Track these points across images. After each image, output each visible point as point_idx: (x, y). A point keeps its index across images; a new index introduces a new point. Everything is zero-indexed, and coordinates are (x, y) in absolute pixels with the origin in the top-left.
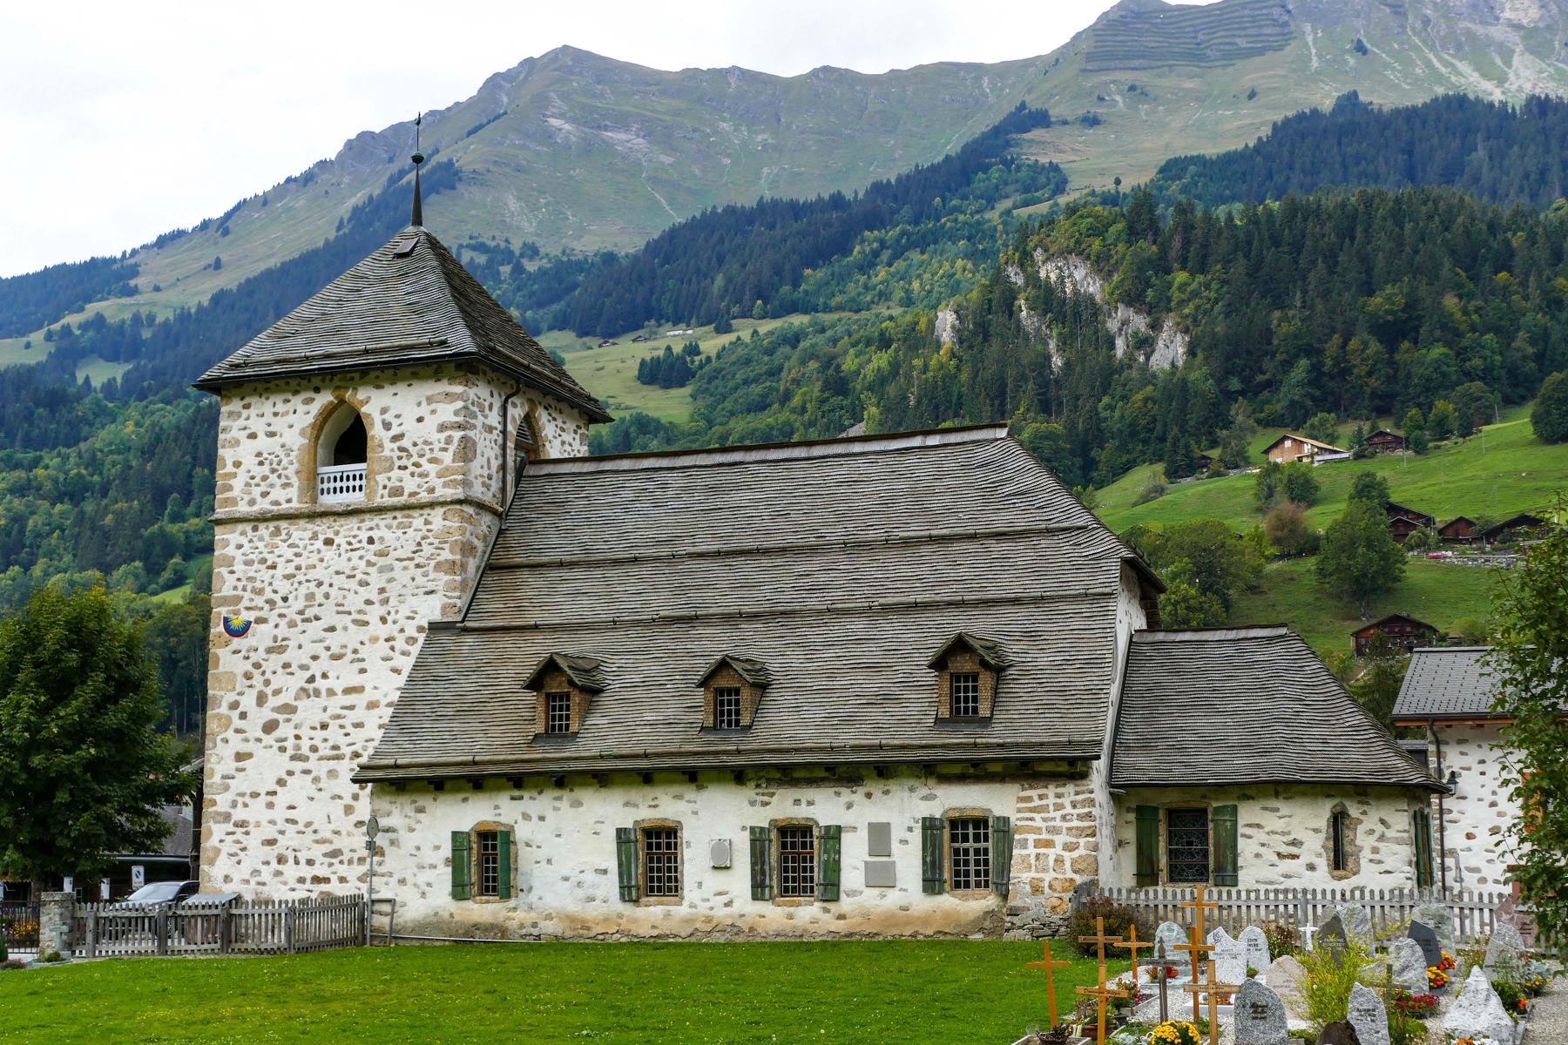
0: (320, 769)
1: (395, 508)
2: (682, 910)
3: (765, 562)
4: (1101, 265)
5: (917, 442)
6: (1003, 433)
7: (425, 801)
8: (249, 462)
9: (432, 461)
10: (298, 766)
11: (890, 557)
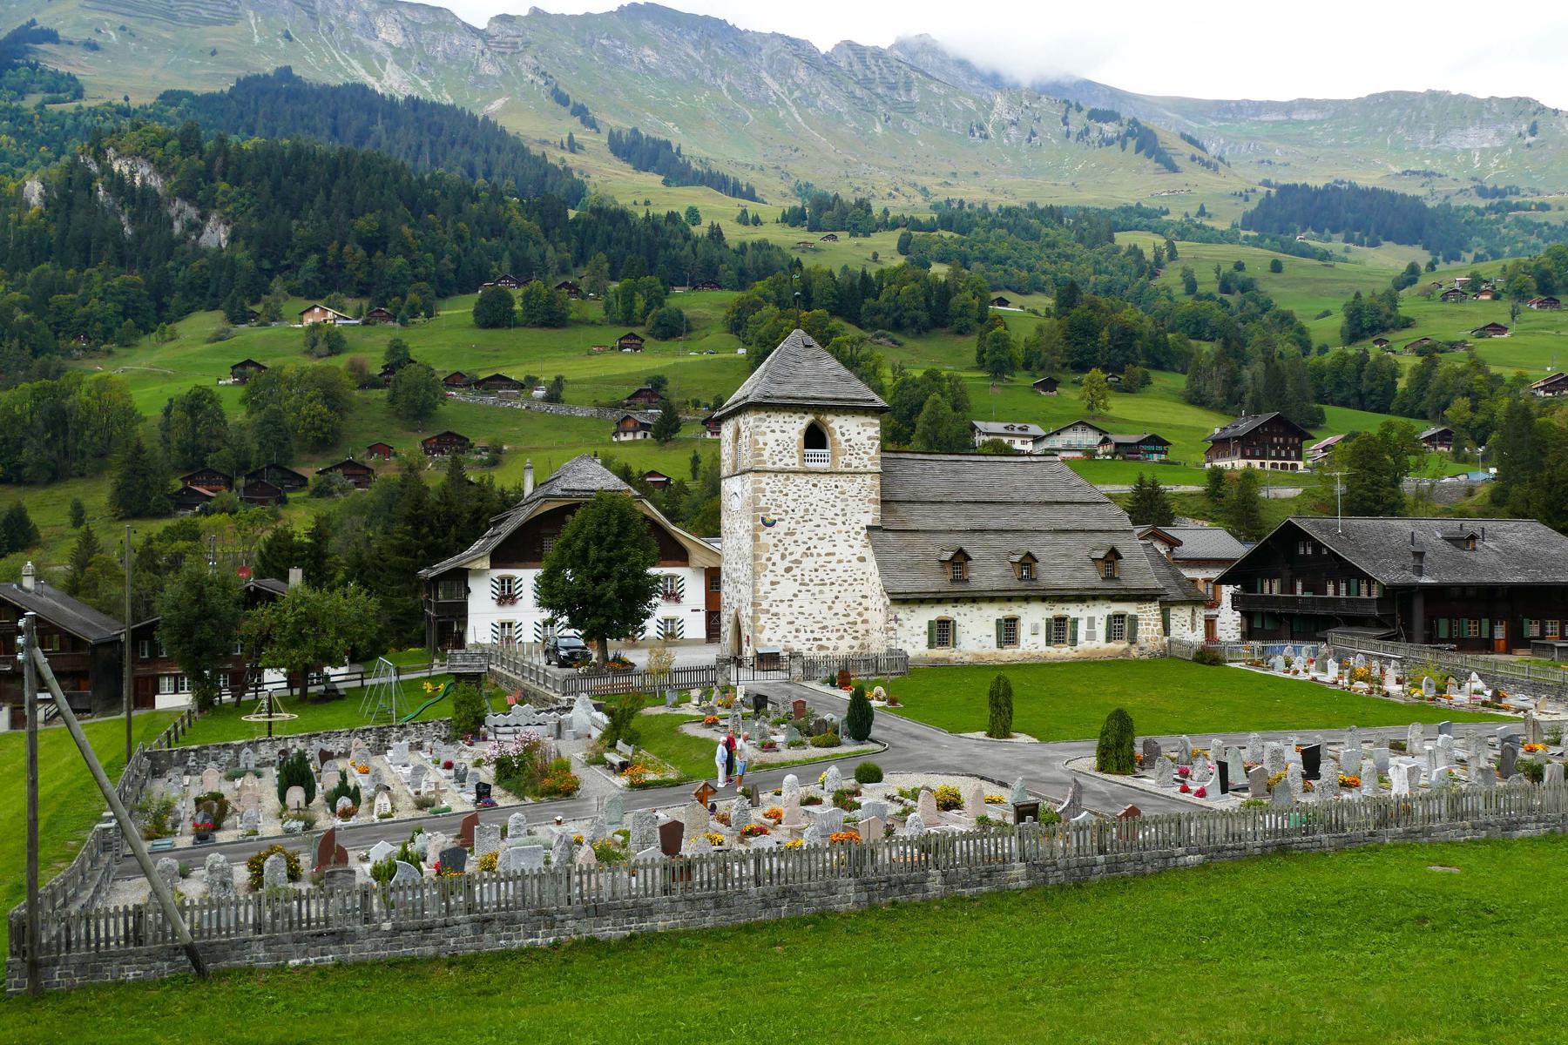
2: (1019, 651)
4: (161, 167)
7: (915, 607)
8: (772, 443)
10: (803, 588)
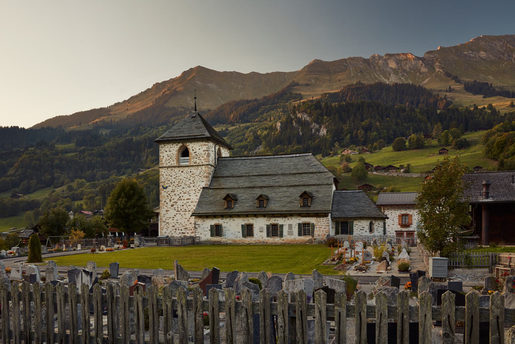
0: (183, 213)
1: (195, 166)
3: (267, 177)
4: (310, 115)
5: (294, 155)
6: (311, 154)
8: (166, 156)
9: (202, 157)
10: (178, 213)
11: (291, 177)
